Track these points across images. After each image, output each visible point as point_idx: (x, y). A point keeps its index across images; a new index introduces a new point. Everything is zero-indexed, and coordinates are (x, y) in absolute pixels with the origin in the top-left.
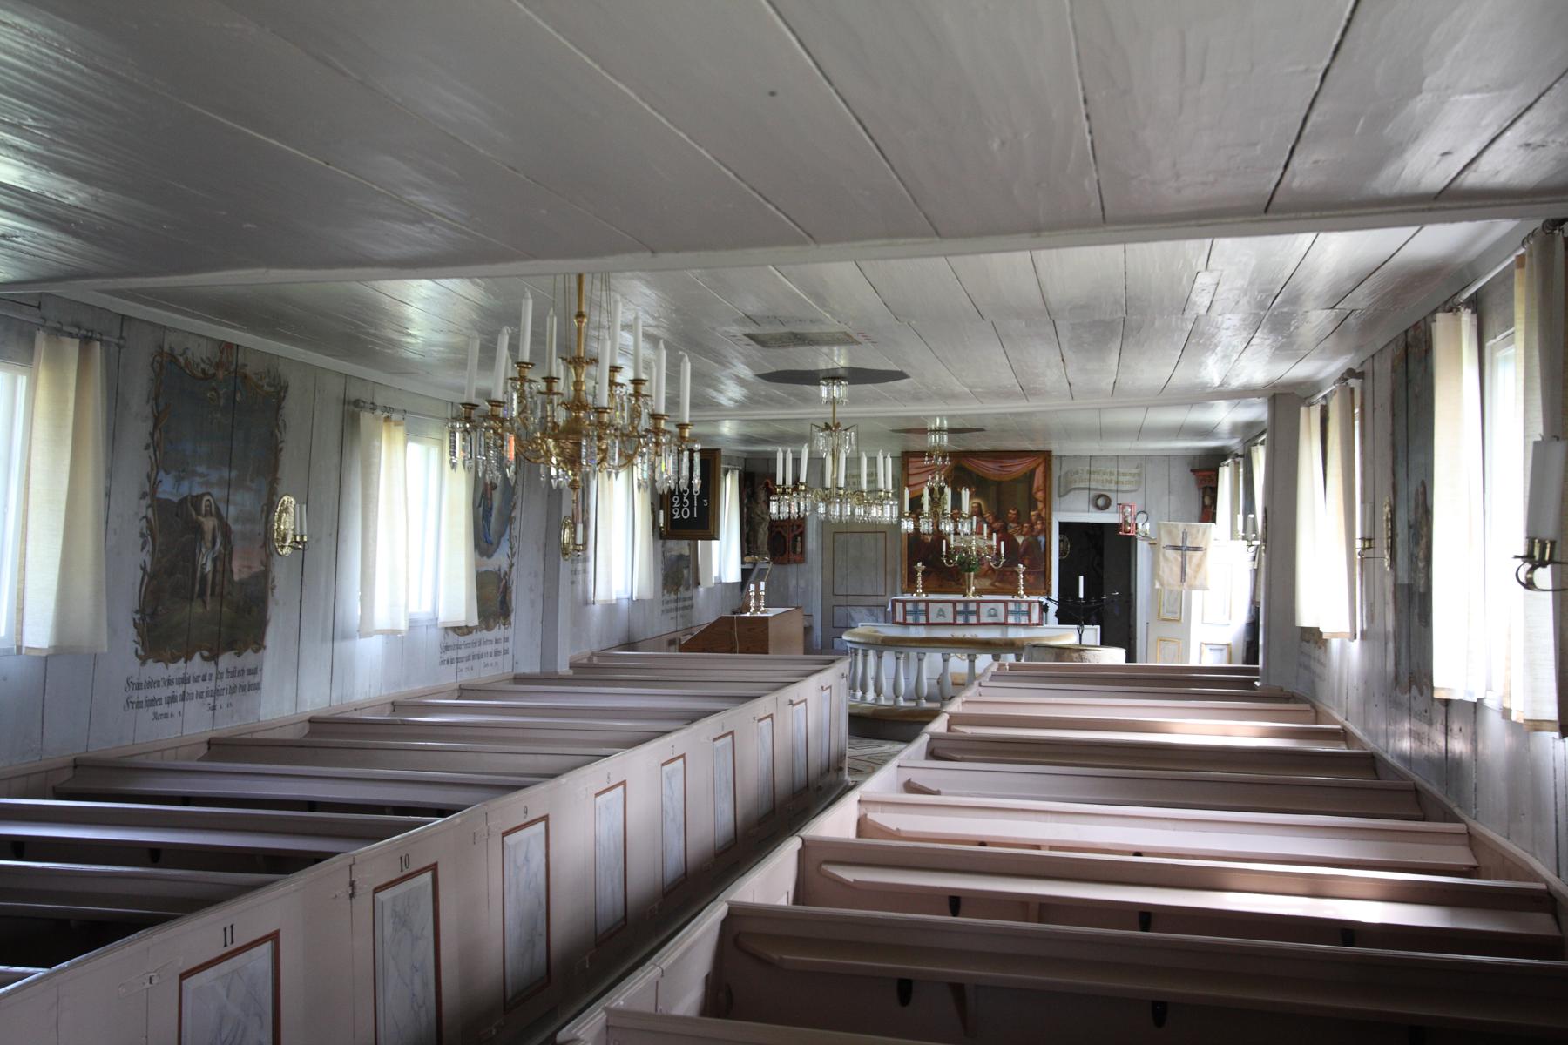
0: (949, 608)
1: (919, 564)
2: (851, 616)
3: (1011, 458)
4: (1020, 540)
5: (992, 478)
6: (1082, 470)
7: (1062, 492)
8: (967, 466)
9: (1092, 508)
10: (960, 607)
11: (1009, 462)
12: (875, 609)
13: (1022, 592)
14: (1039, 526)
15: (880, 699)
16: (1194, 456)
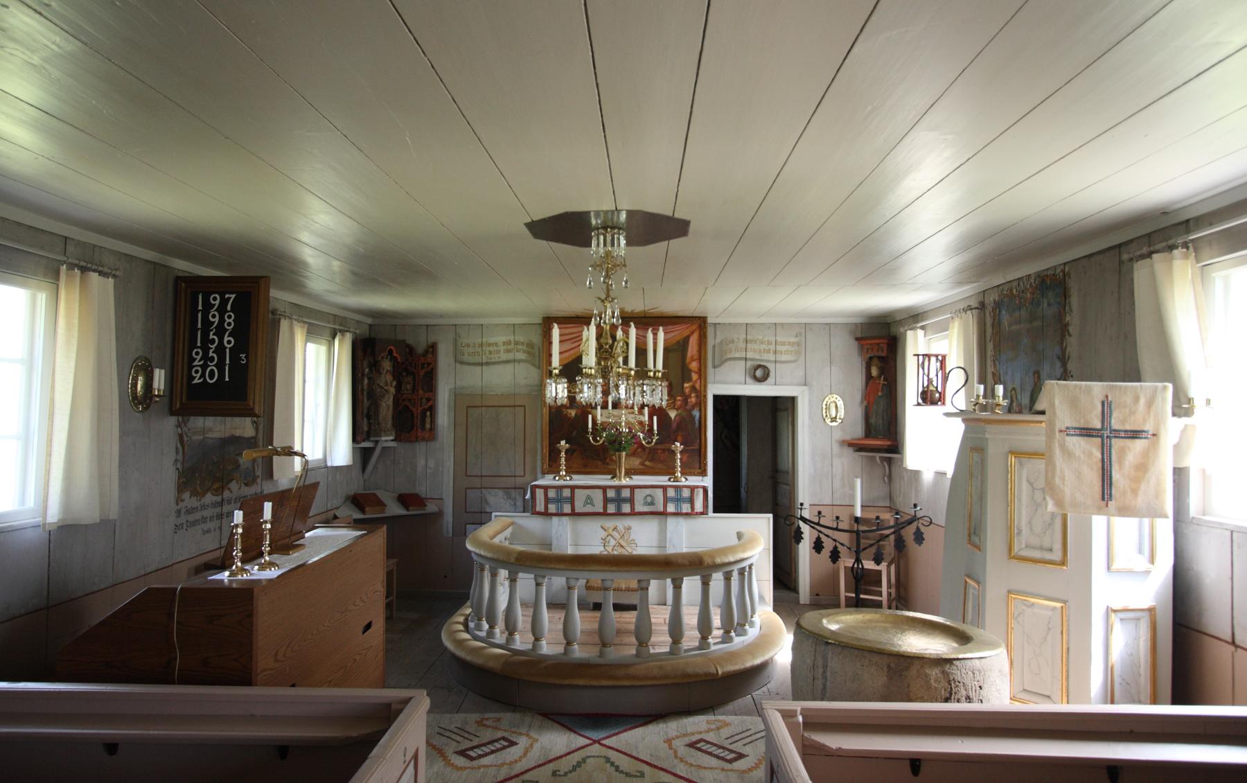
0: (598, 496)
1: (563, 443)
2: (486, 500)
6: (738, 339)
9: (749, 380)
10: (611, 494)
12: (513, 493)
13: (679, 475)
15: (513, 640)
16: (856, 325)
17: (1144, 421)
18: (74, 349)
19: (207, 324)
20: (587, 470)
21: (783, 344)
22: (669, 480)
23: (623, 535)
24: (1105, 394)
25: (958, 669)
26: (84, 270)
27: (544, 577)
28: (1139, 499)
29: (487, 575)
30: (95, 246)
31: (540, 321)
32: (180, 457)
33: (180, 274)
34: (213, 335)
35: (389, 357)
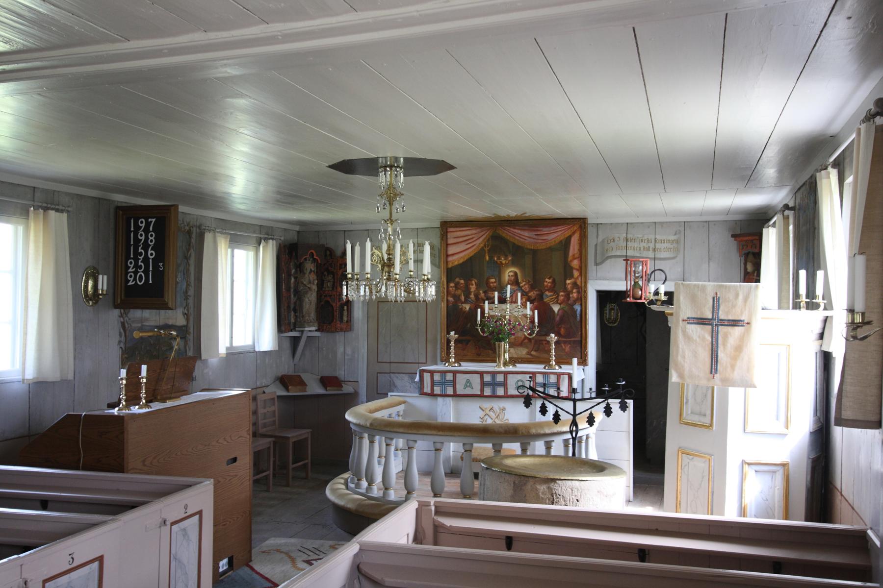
0: (476, 380)
1: (452, 333)
2: (394, 383)
3: (546, 227)
4: (556, 308)
5: (528, 247)
7: (598, 261)
8: (504, 235)
10: (487, 378)
11: (545, 230)
13: (554, 363)
14: (575, 295)
16: (736, 222)
17: (742, 313)
18: (40, 263)
19: (137, 241)
20: (480, 359)
21: (662, 241)
22: (545, 368)
23: (499, 415)
24: (715, 292)
25: (560, 487)
26: (46, 209)
27: (392, 439)
28: (736, 373)
29: (366, 442)
30: (54, 191)
31: (439, 226)
32: (123, 338)
33: (119, 205)
34: (141, 249)
35: (311, 259)
